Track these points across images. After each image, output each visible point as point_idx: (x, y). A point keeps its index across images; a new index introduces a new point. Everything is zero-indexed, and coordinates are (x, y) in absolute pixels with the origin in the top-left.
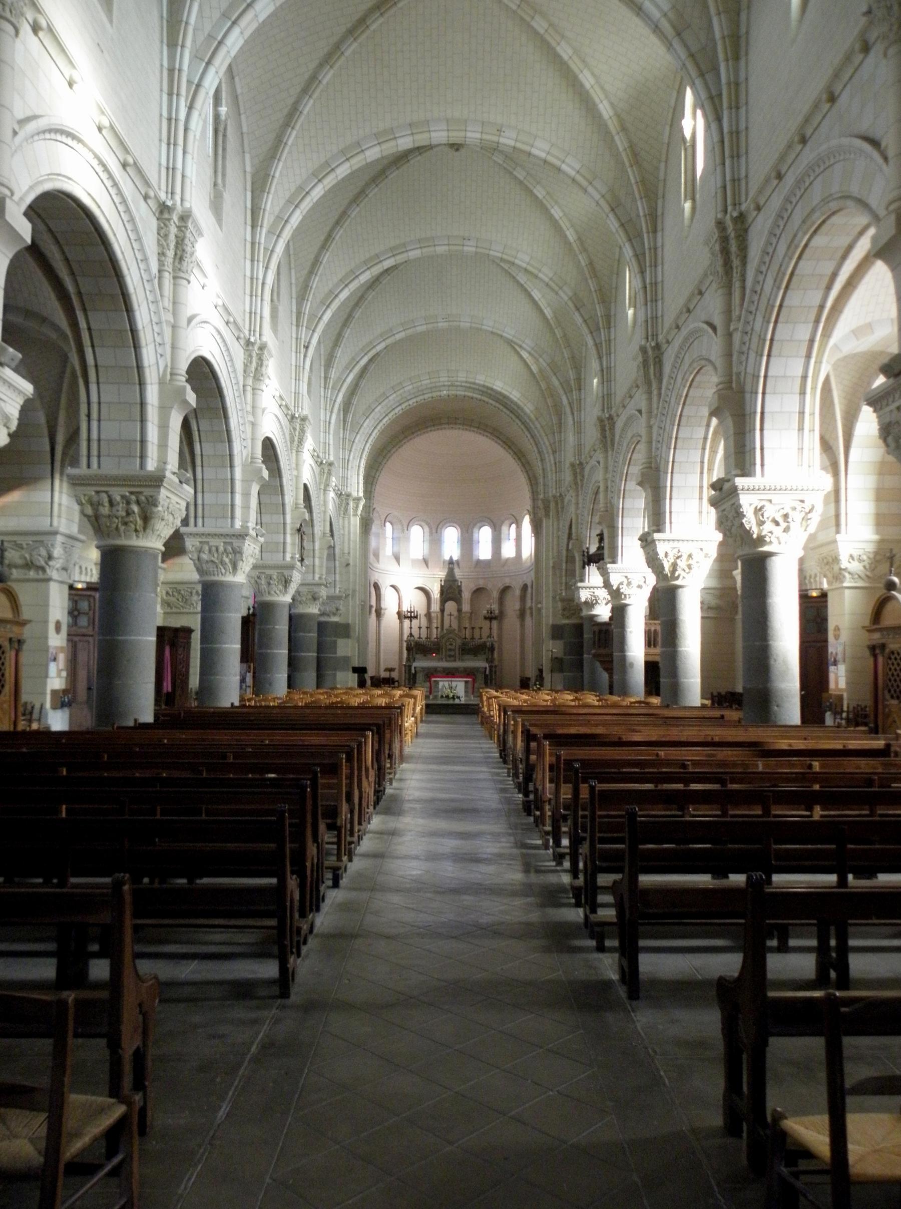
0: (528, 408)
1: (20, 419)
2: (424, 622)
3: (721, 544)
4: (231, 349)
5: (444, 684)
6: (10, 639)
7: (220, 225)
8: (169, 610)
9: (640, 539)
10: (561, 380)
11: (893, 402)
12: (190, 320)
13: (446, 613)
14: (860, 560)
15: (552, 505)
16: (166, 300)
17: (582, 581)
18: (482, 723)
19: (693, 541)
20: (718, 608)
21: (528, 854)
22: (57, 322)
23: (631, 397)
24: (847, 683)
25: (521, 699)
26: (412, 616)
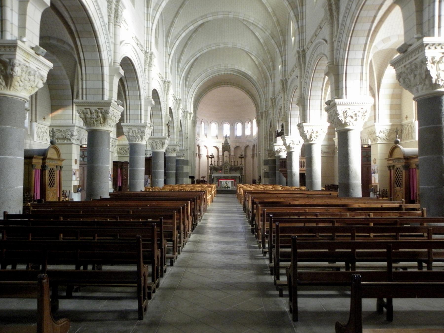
0: (255, 78)
1: (48, 77)
2: (216, 159)
3: (329, 128)
4: (139, 54)
5: (224, 182)
6: (57, 166)
7: (134, 7)
8: (120, 155)
9: (297, 126)
10: (267, 66)
11: (403, 63)
12: (121, 43)
13: (224, 156)
14: (384, 133)
15: (264, 114)
16: (111, 34)
17: (275, 143)
18: (238, 197)
19: (318, 126)
20: (327, 153)
21: (252, 251)
22: (70, 43)
23: (294, 71)
24: (379, 181)
25: (252, 188)
26: (212, 157)
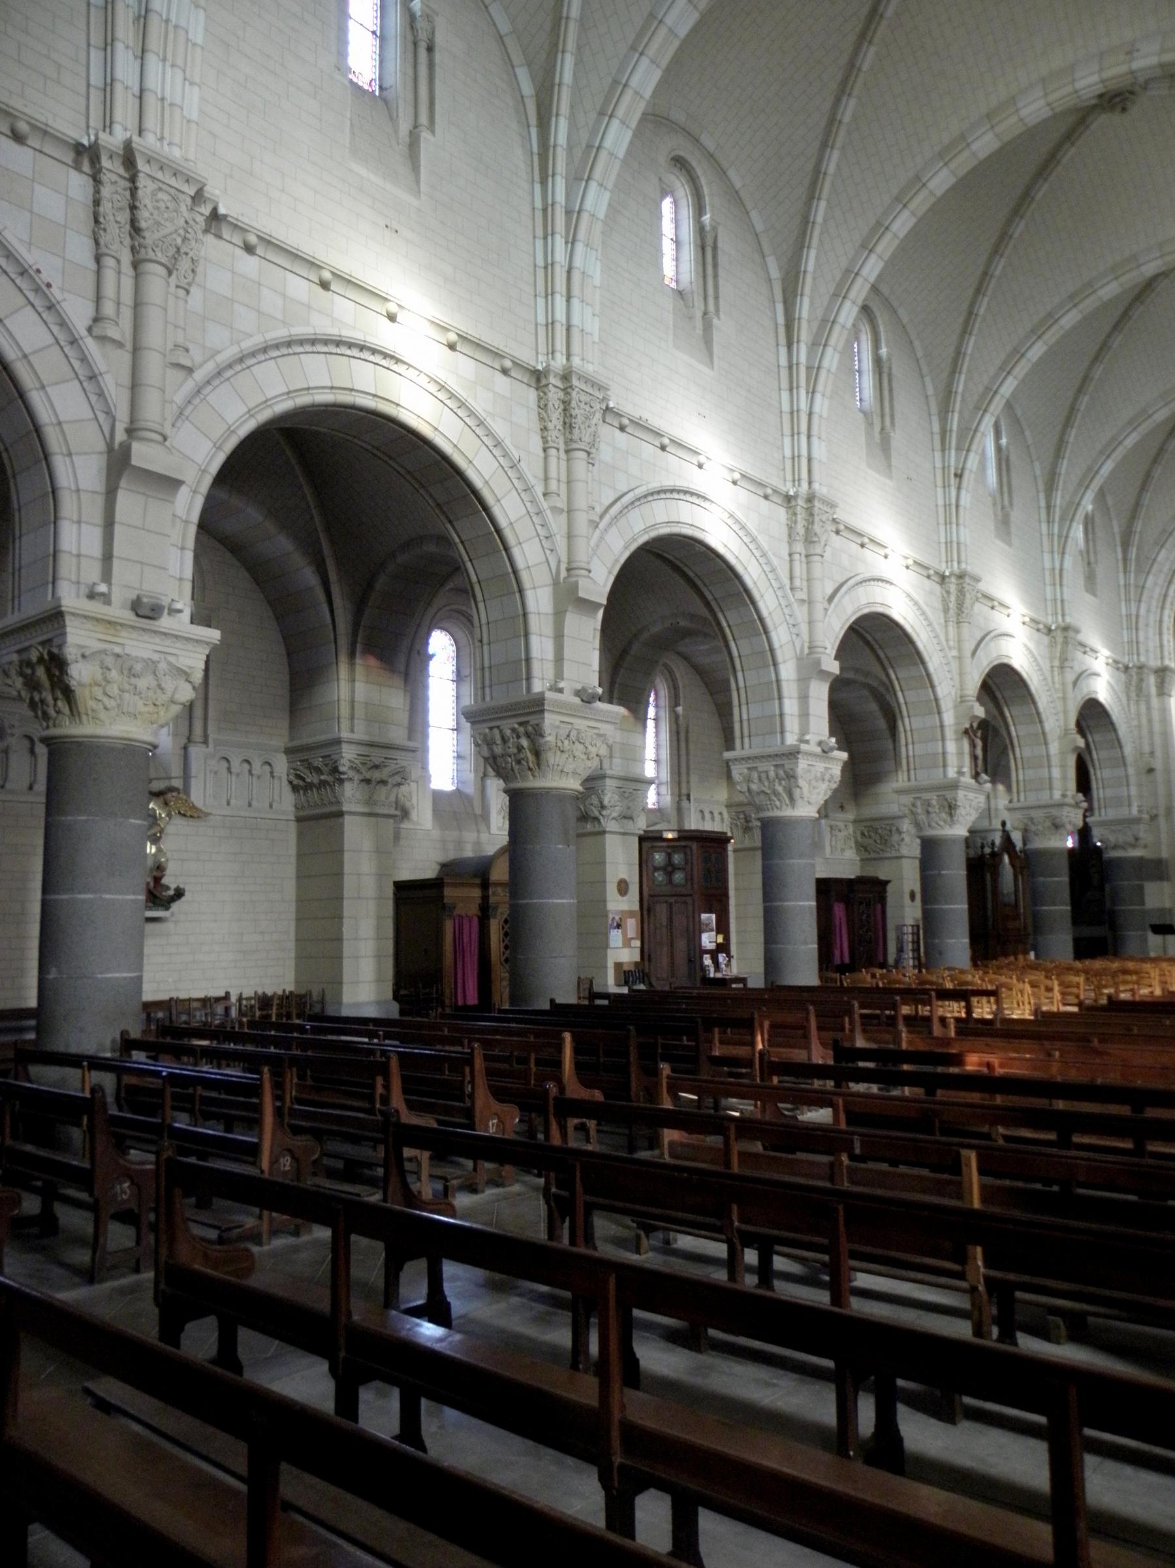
8: (866, 856)
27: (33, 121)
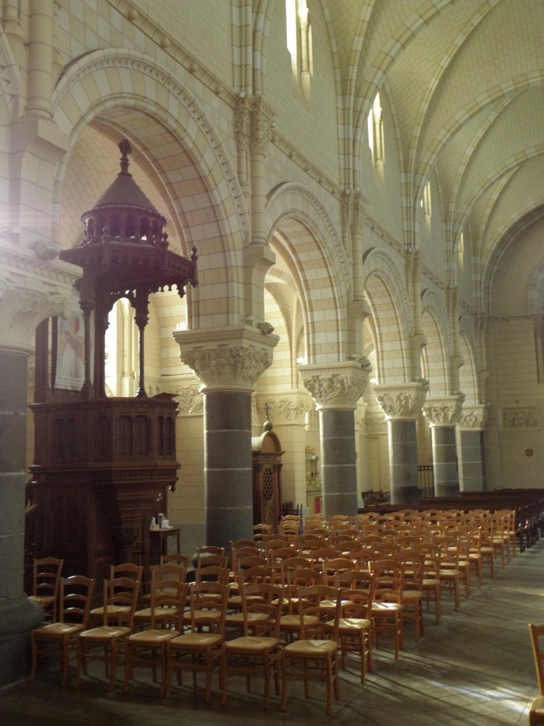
27: (140, 11)
